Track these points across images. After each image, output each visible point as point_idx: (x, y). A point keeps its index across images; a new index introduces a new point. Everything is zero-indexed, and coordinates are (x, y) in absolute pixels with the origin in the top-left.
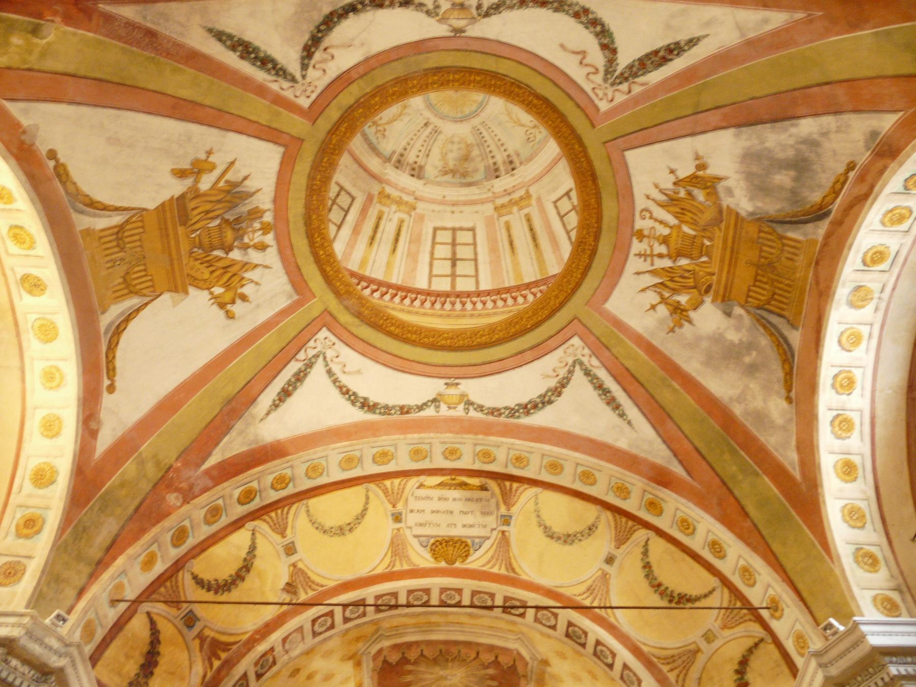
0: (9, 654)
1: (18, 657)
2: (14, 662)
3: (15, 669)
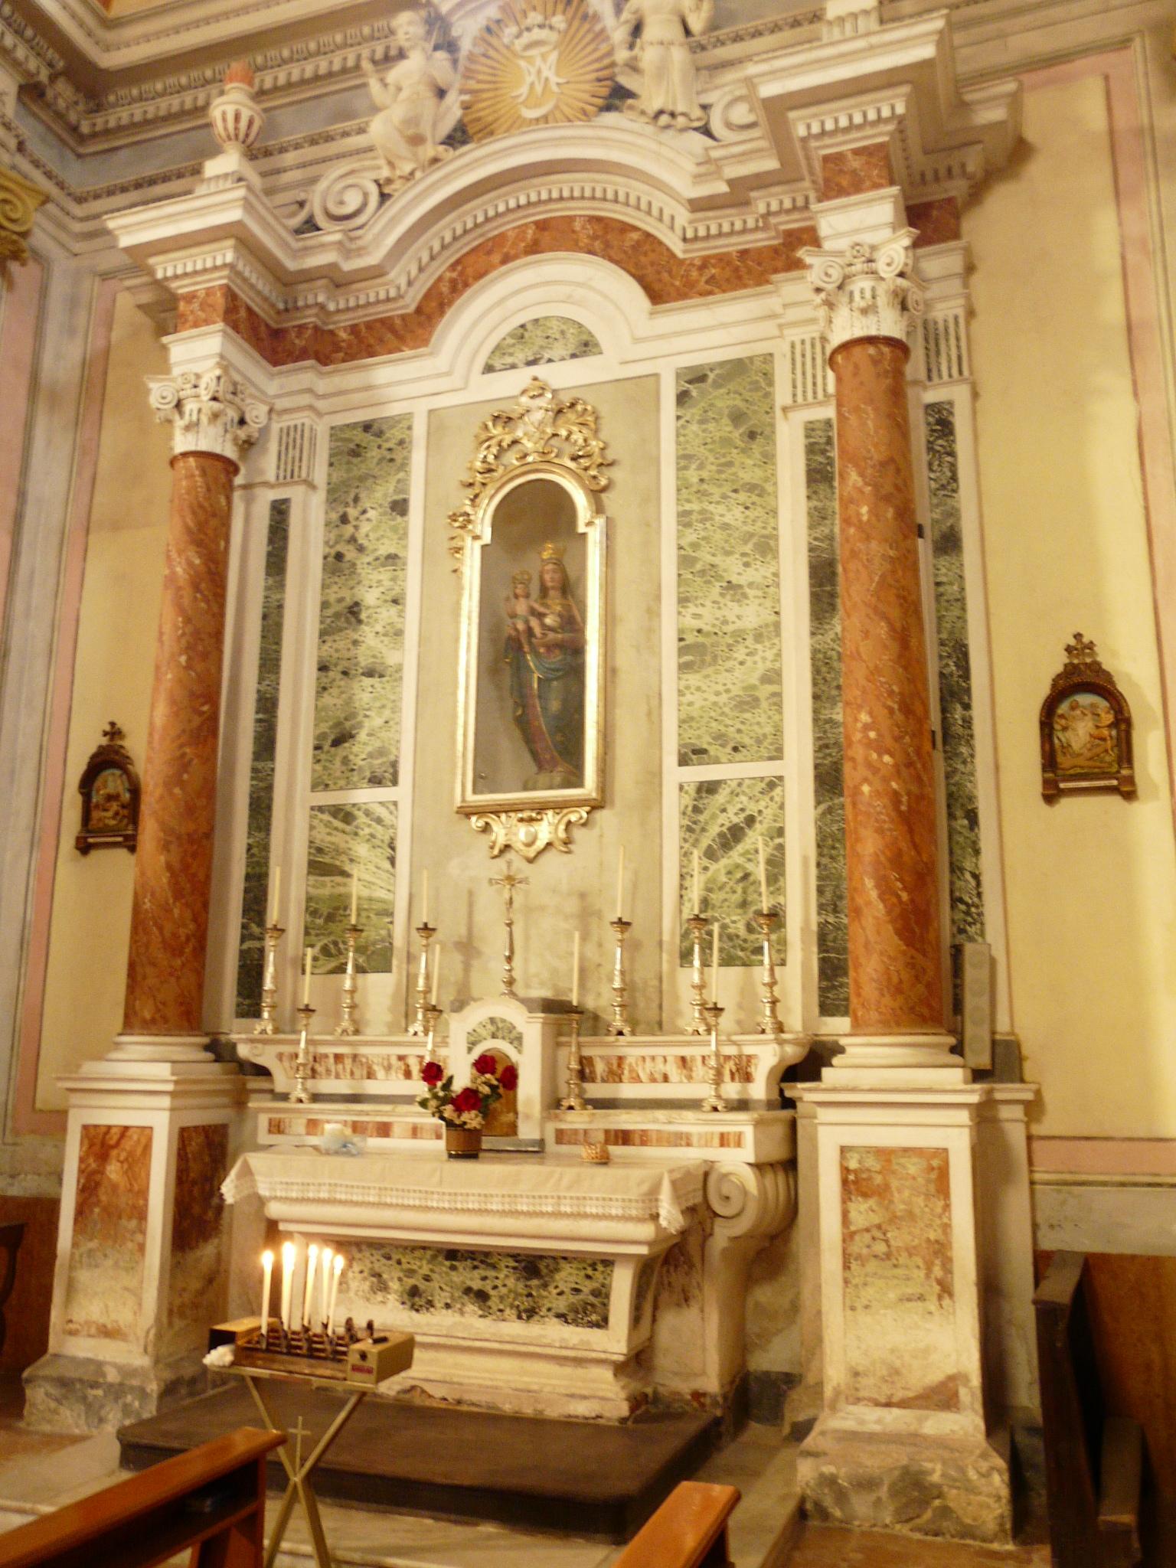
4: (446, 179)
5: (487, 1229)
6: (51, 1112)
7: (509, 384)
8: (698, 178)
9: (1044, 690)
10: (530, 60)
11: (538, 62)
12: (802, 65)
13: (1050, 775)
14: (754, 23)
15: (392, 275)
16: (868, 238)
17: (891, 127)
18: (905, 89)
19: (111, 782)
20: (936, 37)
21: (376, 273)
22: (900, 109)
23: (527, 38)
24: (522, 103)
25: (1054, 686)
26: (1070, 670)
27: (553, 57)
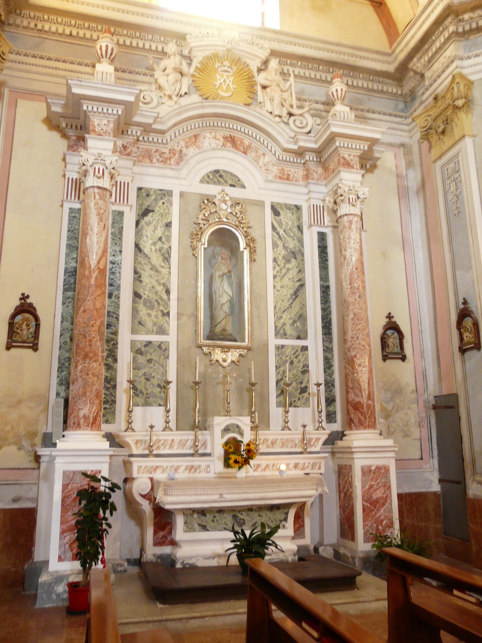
0: (457, 16)
1: (465, 12)
2: (466, 16)
3: (472, 18)
4: (246, 112)
5: (388, 453)
6: (461, 435)
7: (212, 190)
8: (288, 142)
9: (11, 311)
10: (222, 76)
11: (225, 77)
12: (341, 125)
13: (10, 340)
14: (80, 60)
15: (167, 134)
16: (104, 153)
17: (362, 152)
18: (123, 107)
19: (468, 322)
20: (136, 95)
21: (163, 132)
22: (120, 113)
23: (223, 68)
24: (218, 88)
25: (15, 310)
26: (22, 305)
27: (232, 79)
